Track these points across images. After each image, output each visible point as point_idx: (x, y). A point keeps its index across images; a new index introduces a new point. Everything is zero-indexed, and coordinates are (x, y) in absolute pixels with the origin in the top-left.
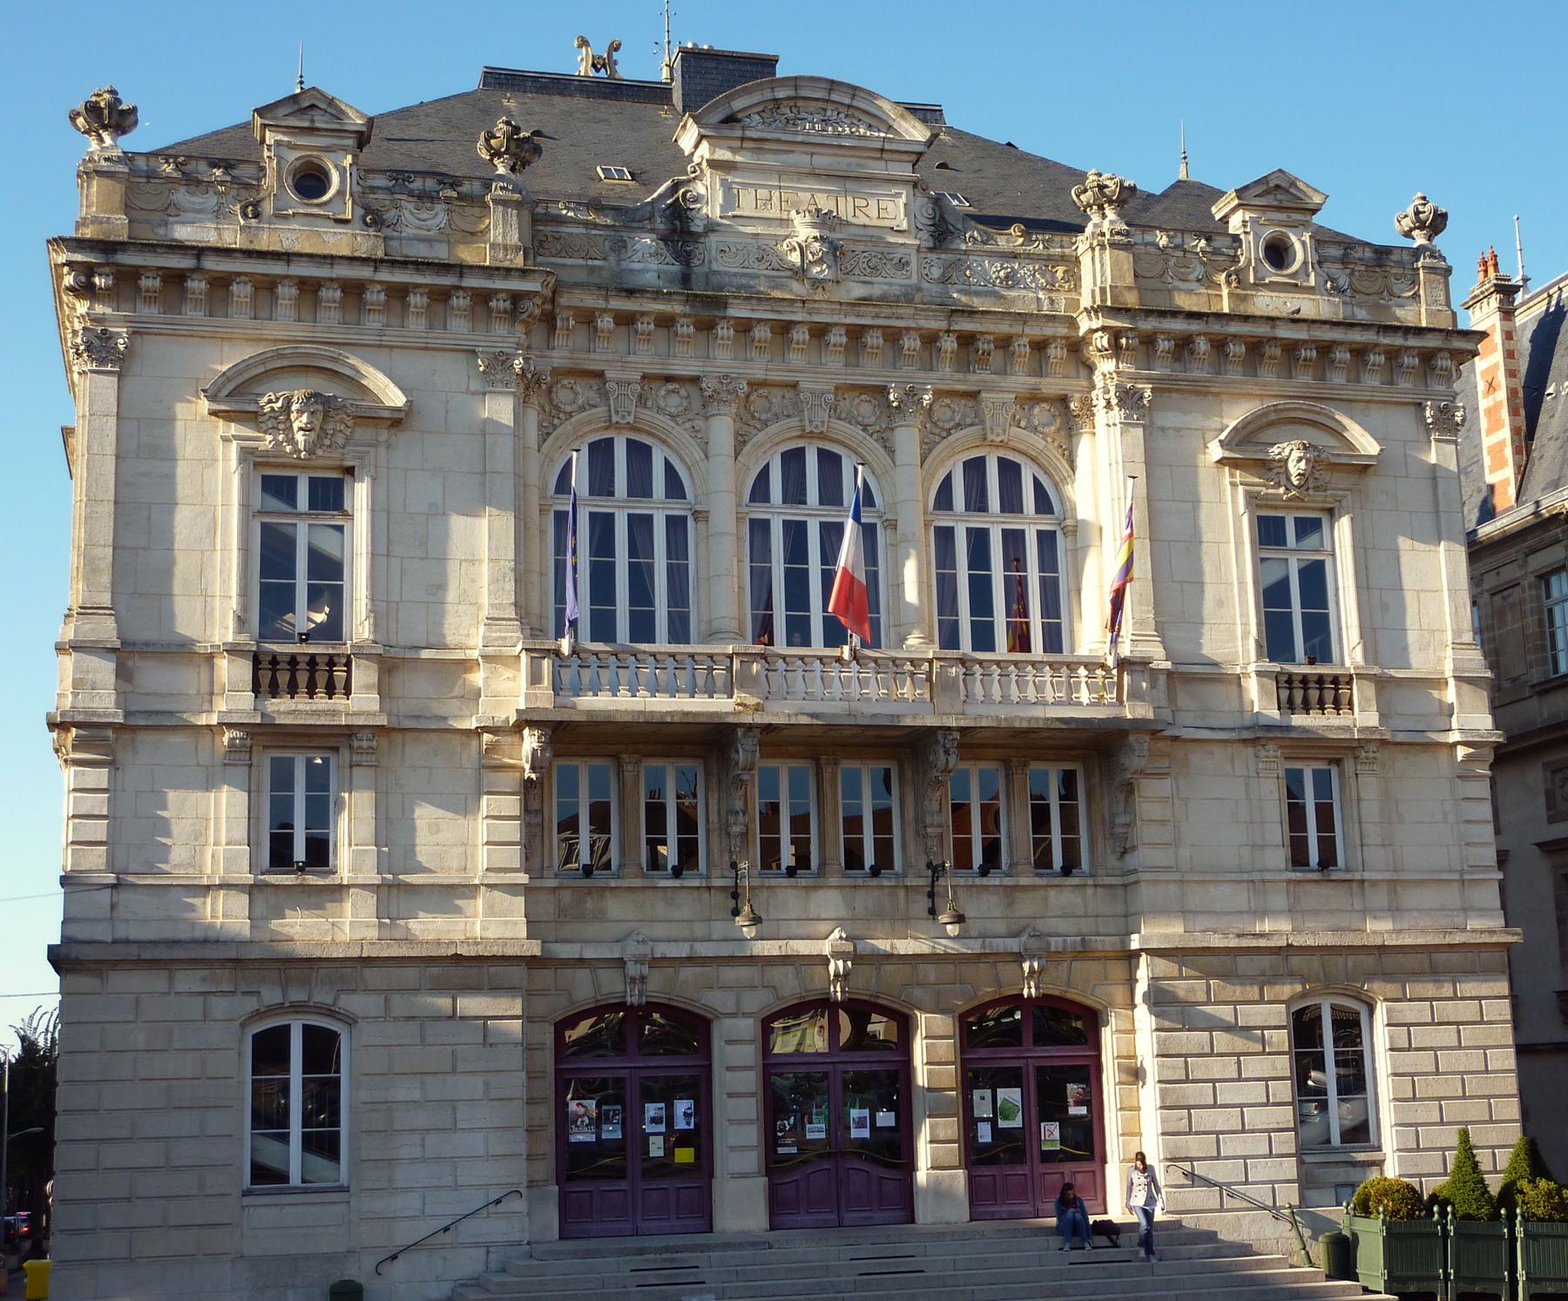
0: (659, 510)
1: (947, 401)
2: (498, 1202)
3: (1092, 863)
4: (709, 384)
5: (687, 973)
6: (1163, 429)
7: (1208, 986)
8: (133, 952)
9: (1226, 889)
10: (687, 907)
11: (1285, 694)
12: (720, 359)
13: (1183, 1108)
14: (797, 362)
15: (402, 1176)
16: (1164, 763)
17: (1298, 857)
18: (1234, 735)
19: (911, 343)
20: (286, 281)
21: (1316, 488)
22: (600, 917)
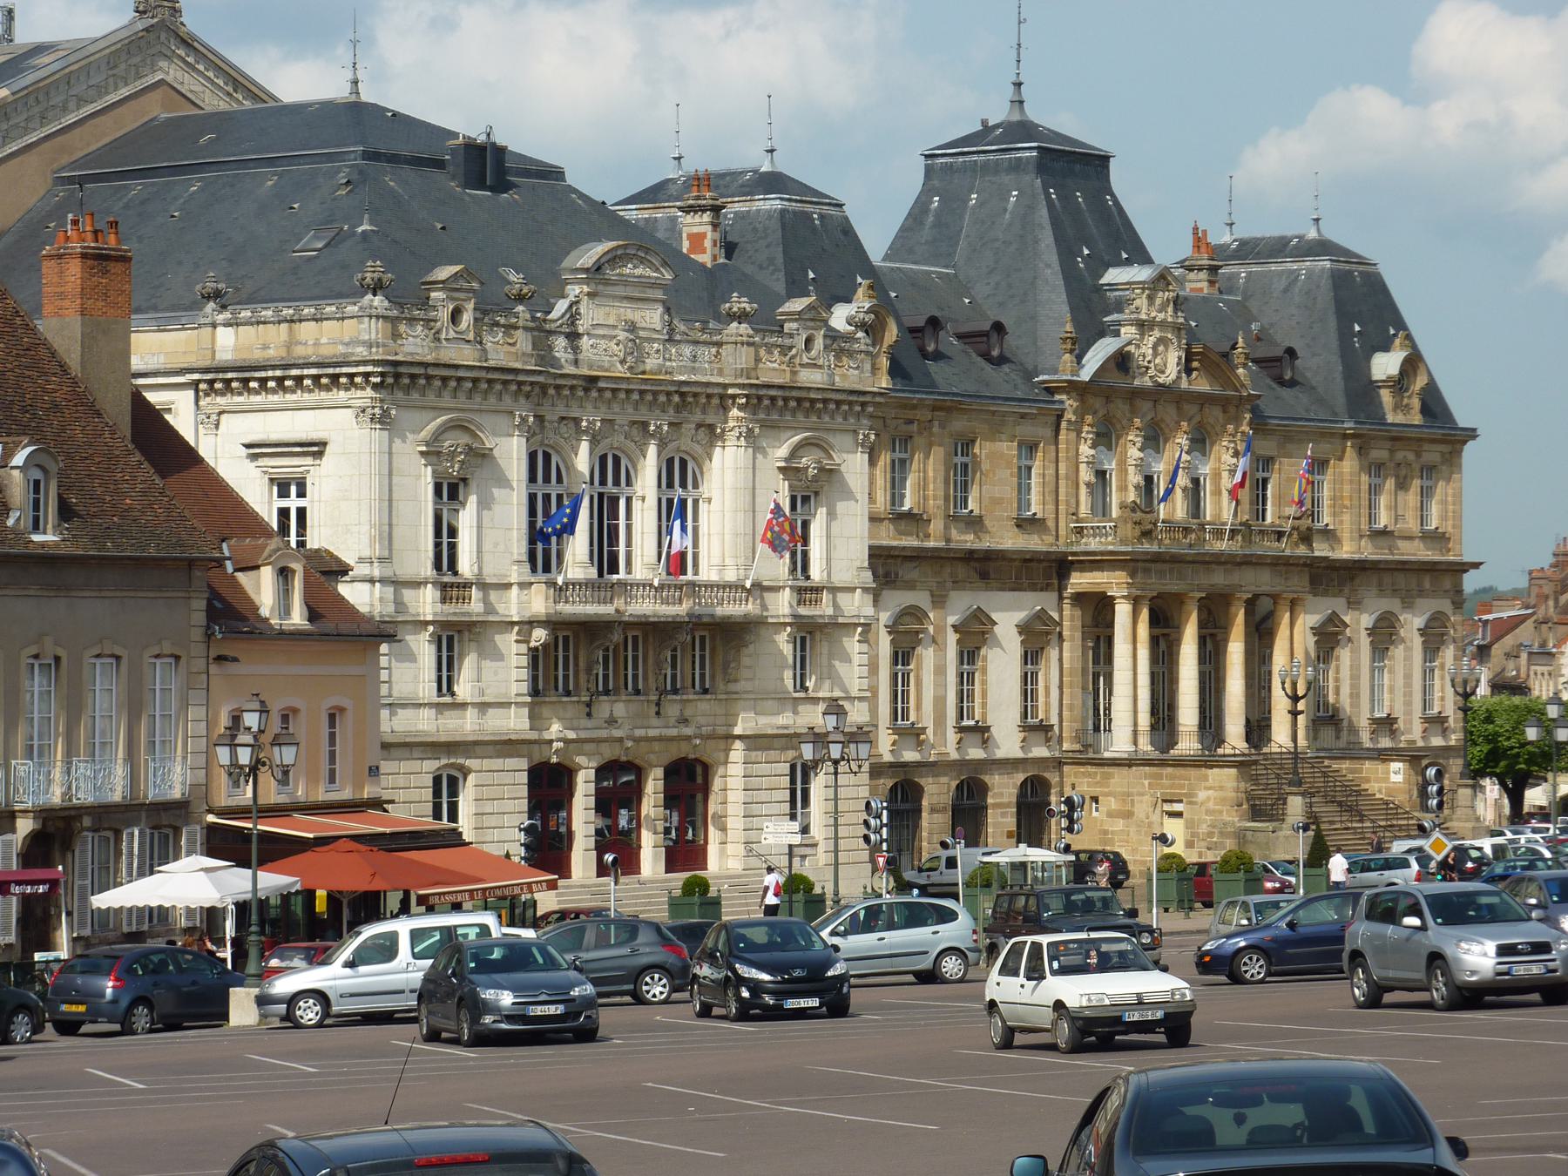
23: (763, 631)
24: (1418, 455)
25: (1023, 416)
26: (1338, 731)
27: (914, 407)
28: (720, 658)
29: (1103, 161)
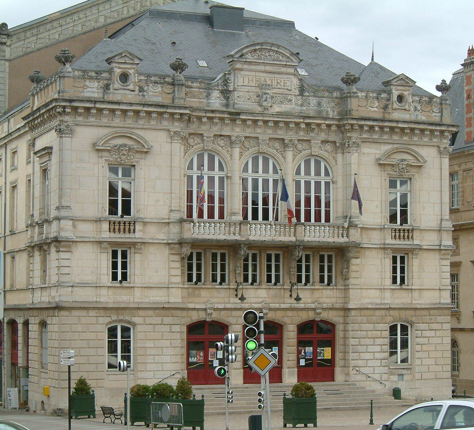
0: (217, 174)
1: (301, 142)
2: (174, 375)
3: (336, 282)
4: (233, 138)
5: (223, 313)
6: (364, 154)
7: (449, 350)
8: (78, 305)
9: (374, 291)
10: (223, 293)
11: (393, 234)
12: (237, 131)
13: (358, 352)
14: (259, 132)
15: (149, 367)
16: (358, 254)
17: (394, 281)
18: (379, 246)
20: (118, 110)
21: (407, 172)
22: (199, 296)
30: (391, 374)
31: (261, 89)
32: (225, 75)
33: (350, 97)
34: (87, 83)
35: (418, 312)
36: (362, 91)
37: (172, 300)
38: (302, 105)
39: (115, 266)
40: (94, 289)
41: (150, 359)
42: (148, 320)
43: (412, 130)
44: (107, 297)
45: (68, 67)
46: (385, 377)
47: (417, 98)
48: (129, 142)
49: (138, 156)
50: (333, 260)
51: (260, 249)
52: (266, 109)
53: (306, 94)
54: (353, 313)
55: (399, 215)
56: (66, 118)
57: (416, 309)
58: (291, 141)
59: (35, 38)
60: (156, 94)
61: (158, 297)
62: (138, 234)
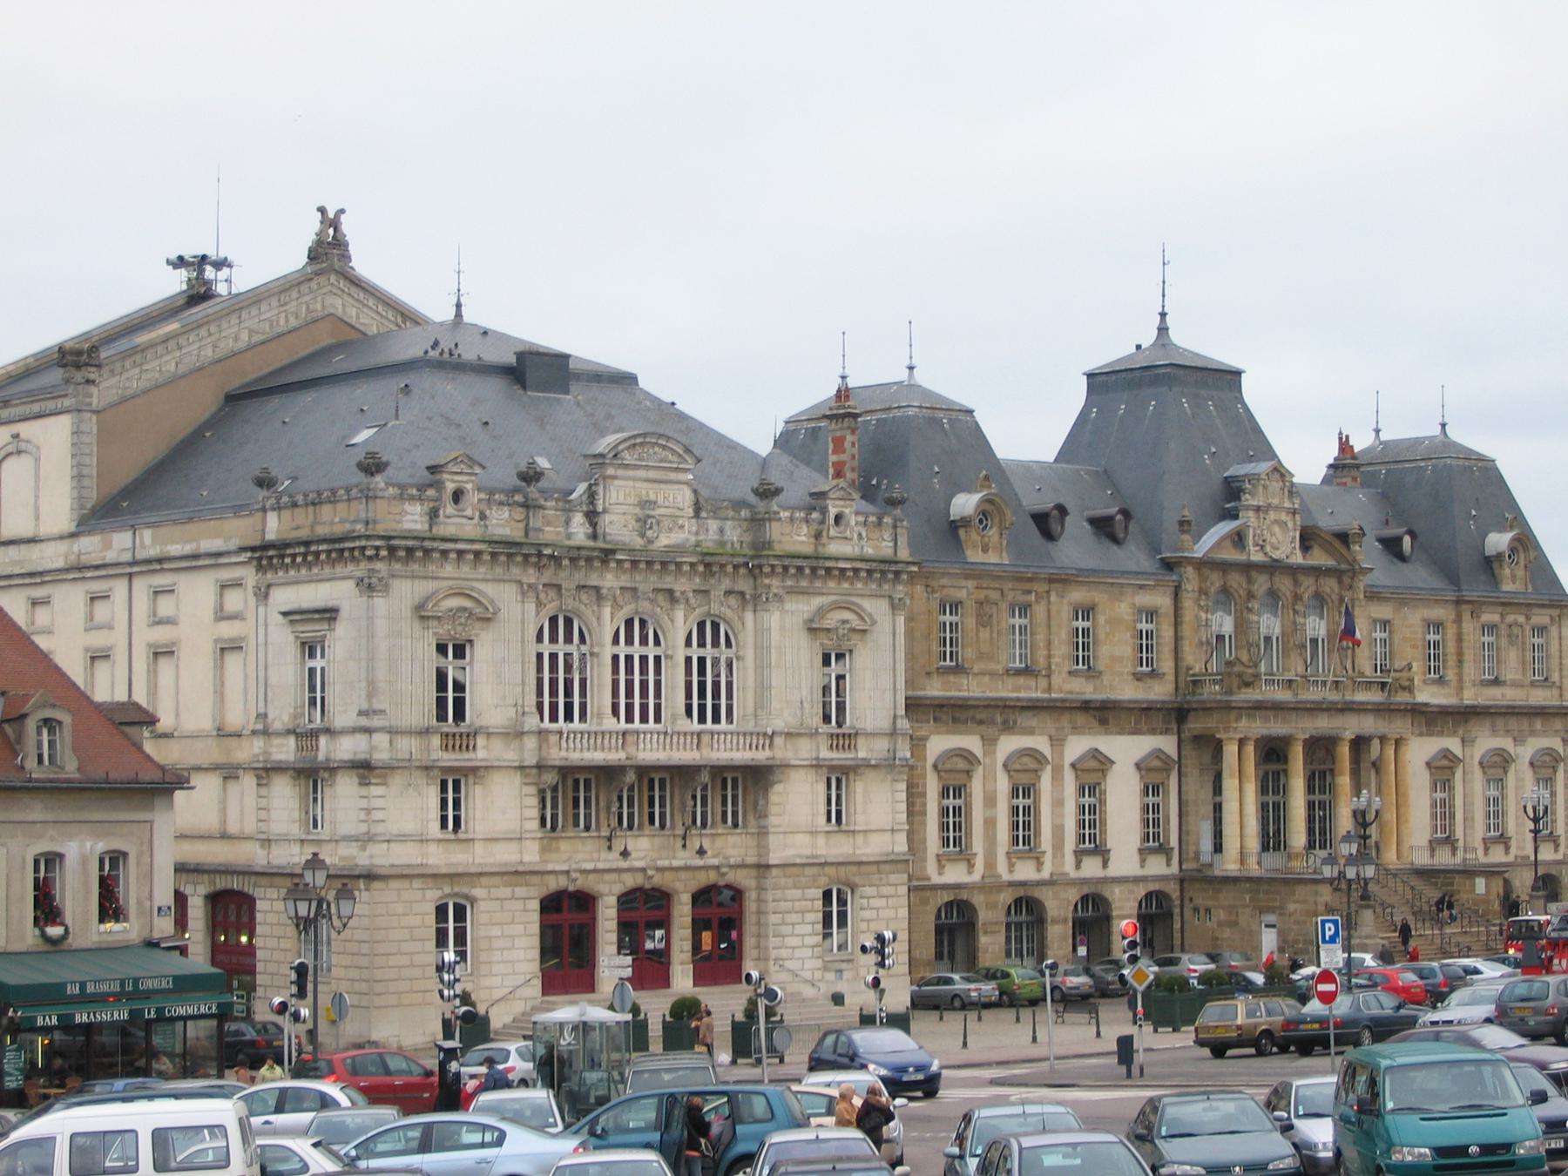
4: (604, 591)
5: (591, 877)
9: (801, 835)
10: (590, 846)
15: (496, 968)
19: (686, 568)
22: (557, 850)
23: (777, 771)
24: (1528, 618)
25: (1141, 587)
26: (1454, 850)
27: (1030, 580)
28: (751, 797)
29: (1237, 374)
30: (825, 969)
31: (643, 508)
32: (590, 486)
33: (770, 520)
34: (407, 507)
35: (864, 869)
36: (785, 509)
37: (527, 858)
38: (697, 533)
39: (444, 802)
40: (418, 845)
41: (496, 956)
42: (495, 893)
43: (856, 570)
44: (438, 857)
45: (379, 481)
46: (818, 975)
47: (861, 519)
48: (468, 604)
49: (478, 625)
50: (745, 785)
51: (650, 776)
52: (650, 542)
53: (704, 514)
54: (774, 872)
55: (833, 706)
56: (379, 566)
57: (860, 863)
58: (683, 593)
59: (137, 370)
60: (503, 523)
61: (505, 855)
62: (481, 754)
